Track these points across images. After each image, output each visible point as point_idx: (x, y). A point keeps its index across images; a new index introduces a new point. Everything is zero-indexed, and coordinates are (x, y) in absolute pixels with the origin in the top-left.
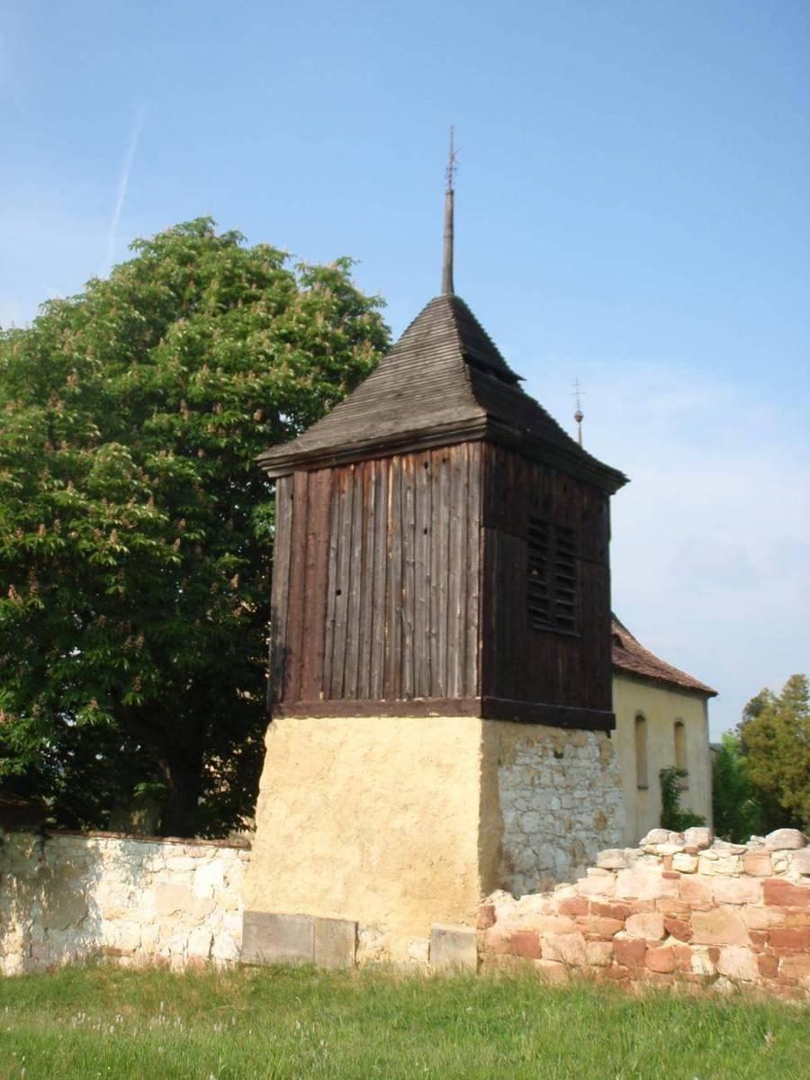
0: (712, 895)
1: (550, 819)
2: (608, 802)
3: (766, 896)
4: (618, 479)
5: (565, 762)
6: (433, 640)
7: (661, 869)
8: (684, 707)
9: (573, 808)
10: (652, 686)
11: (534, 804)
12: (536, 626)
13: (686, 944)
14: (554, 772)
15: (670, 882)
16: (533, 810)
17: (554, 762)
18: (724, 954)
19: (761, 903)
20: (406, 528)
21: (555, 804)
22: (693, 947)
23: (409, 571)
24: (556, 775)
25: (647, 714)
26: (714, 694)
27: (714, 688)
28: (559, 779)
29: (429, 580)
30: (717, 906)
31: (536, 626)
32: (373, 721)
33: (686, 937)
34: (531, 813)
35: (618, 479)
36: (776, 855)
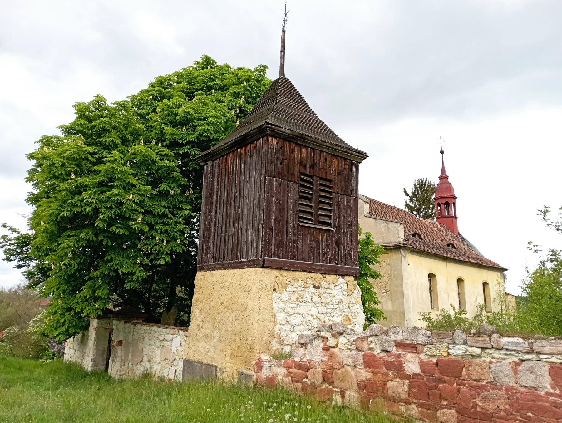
0: (342, 360)
1: (310, 318)
2: (352, 311)
3: (364, 362)
4: (363, 156)
5: (321, 290)
6: (248, 232)
7: (322, 345)
8: (492, 277)
9: (326, 313)
10: (467, 265)
11: (298, 310)
12: (301, 224)
13: (331, 387)
14: (313, 295)
15: (325, 352)
16: (297, 313)
17: (314, 290)
18: (347, 393)
19: (362, 367)
20: (241, 180)
21: (314, 311)
22: (334, 389)
23: (242, 200)
24: (314, 296)
25: (464, 277)
26: (506, 270)
27: (505, 267)
28: (316, 299)
29: (248, 203)
30: (343, 367)
31: (301, 224)
32: (227, 271)
33: (331, 383)
34: (296, 315)
35: (363, 156)
36: (370, 339)
